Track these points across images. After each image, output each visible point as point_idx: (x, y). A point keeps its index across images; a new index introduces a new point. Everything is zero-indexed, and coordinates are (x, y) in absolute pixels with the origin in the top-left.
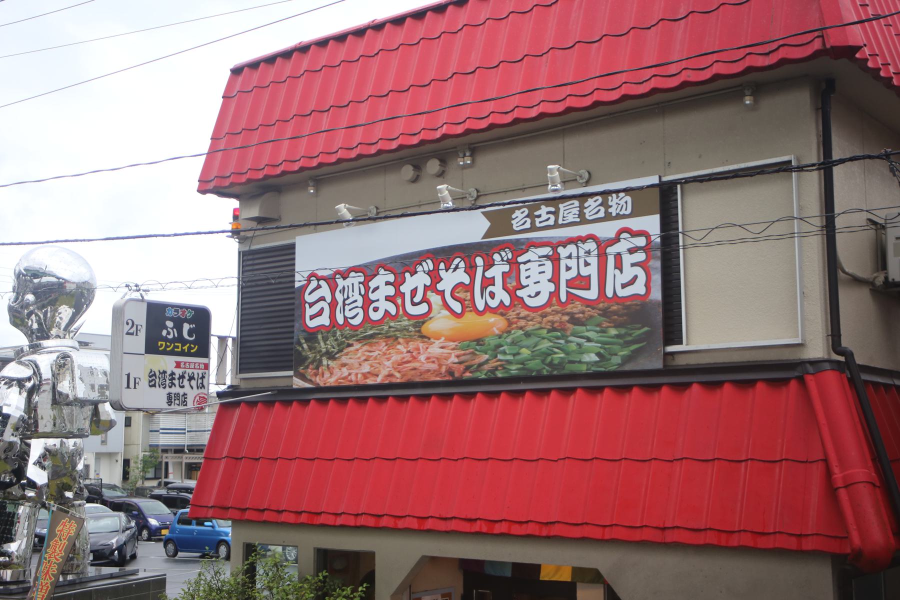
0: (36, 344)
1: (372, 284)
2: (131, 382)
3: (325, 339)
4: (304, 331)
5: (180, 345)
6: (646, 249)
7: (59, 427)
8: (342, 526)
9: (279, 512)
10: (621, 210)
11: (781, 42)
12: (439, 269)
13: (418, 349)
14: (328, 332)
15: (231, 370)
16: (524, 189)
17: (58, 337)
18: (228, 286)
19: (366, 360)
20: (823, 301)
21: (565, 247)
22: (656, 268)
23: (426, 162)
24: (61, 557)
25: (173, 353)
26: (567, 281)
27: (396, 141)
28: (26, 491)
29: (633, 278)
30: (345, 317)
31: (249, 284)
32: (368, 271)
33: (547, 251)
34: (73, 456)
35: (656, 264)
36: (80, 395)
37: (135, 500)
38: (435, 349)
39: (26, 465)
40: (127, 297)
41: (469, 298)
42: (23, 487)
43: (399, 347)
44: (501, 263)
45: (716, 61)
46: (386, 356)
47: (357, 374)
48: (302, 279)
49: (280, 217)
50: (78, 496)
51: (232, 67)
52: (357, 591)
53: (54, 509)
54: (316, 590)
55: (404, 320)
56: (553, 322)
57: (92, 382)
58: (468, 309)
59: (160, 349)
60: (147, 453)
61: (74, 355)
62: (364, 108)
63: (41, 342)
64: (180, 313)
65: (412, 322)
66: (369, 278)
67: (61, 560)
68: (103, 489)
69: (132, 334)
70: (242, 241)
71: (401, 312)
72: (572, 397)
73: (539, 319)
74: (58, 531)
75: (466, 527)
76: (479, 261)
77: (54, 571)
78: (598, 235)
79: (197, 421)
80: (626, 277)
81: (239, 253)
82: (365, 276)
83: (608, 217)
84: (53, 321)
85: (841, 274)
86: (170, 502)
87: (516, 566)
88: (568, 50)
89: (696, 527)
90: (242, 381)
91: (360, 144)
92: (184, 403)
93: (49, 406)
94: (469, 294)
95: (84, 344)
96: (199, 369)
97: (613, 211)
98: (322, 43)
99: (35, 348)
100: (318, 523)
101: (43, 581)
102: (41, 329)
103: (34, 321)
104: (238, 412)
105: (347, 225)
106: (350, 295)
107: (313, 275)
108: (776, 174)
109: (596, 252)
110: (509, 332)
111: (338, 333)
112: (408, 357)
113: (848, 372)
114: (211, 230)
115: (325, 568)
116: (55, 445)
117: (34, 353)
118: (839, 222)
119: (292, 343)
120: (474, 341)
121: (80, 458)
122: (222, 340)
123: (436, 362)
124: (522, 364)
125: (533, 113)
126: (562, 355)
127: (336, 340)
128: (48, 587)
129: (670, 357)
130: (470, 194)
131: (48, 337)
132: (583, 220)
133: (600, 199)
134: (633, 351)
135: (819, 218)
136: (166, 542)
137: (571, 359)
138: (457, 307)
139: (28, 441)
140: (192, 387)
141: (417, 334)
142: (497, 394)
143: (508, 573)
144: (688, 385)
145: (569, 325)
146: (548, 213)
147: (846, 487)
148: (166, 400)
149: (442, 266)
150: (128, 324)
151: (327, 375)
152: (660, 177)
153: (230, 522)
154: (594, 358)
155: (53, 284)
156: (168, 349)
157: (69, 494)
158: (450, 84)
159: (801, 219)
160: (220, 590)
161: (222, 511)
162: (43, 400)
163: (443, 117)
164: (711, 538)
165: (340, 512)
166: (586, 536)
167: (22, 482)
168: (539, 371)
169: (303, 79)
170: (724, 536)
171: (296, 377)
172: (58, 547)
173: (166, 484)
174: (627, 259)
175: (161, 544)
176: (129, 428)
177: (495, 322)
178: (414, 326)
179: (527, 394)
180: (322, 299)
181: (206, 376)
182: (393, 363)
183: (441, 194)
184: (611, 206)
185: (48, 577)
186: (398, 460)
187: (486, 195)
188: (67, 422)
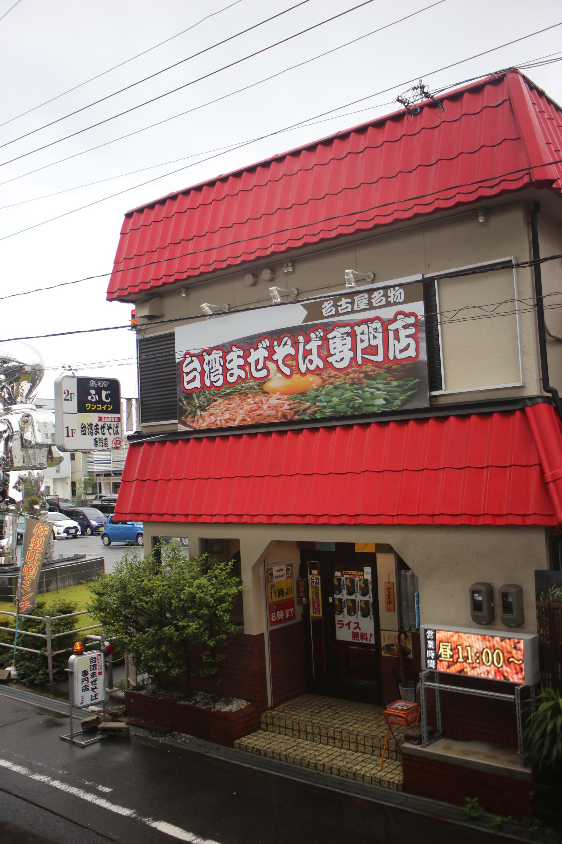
0: (8, 408)
1: (228, 358)
2: (69, 432)
3: (198, 397)
4: (183, 392)
5: (100, 405)
6: (415, 325)
7: (27, 463)
8: (216, 523)
9: (174, 515)
10: (397, 299)
11: (502, 179)
12: (273, 346)
13: (262, 401)
14: (200, 392)
15: (136, 421)
16: (329, 287)
17: (22, 402)
18: (130, 364)
19: (226, 410)
20: (536, 356)
21: (359, 326)
22: (422, 338)
23: (261, 272)
24: (42, 549)
25: (96, 411)
26: (362, 349)
27: (239, 258)
28: (9, 506)
29: (407, 345)
30: (211, 381)
31: (144, 362)
32: (225, 349)
33: (347, 329)
34: (37, 482)
35: (422, 335)
36: (39, 441)
37: (81, 509)
38: (273, 401)
39: (8, 488)
40: (63, 375)
41: (295, 364)
42: (7, 503)
43: (249, 400)
44: (316, 339)
45: (458, 193)
46: (241, 407)
47: (221, 420)
48: (180, 357)
49: (163, 315)
50: (42, 507)
51: (125, 212)
52: (228, 565)
53: (28, 517)
54: (202, 565)
55: (251, 382)
56: (353, 379)
57: (46, 432)
58: (295, 372)
59: (88, 409)
60: (86, 477)
61: (33, 414)
62: (217, 237)
63: (11, 406)
64: (99, 384)
65: (257, 382)
66: (226, 354)
67: (42, 551)
68: (60, 502)
69: (68, 400)
70: (138, 332)
71: (249, 376)
72: (368, 429)
73: (344, 377)
74: (35, 532)
75: (300, 520)
76: (301, 339)
77: (39, 558)
78: (382, 317)
79: (118, 454)
80: (402, 345)
81: (137, 340)
82: (223, 353)
83: (388, 304)
84: (18, 392)
85: (548, 337)
86: (104, 509)
87: (338, 545)
88: (356, 190)
89: (454, 513)
90: (144, 428)
91: (215, 261)
92: (106, 445)
93: (20, 449)
94: (295, 362)
95: (39, 407)
96: (115, 421)
97: (391, 300)
98: (186, 193)
99: (7, 411)
100: (200, 522)
101: (32, 565)
102: (10, 398)
103: (6, 393)
104: (142, 449)
105: (209, 318)
106: (214, 366)
107: (188, 353)
108: (502, 270)
109: (381, 329)
110: (324, 387)
111: (207, 393)
112: (255, 407)
113: (554, 404)
114: (117, 326)
115: (207, 551)
116: (25, 475)
117: (7, 414)
118: (546, 302)
119: (176, 401)
120: (299, 394)
121: (42, 483)
122: (129, 400)
123: (274, 409)
124: (334, 408)
125: (334, 234)
126: (360, 401)
127: (206, 397)
128: (36, 569)
129: (434, 399)
130: (293, 293)
131: (15, 403)
132: (371, 307)
133: (382, 292)
134: (409, 396)
135: (532, 299)
136: (103, 536)
137: (367, 403)
138: (287, 371)
139: (8, 473)
140: (110, 434)
141: (260, 391)
142: (317, 429)
143: (333, 549)
144: (447, 418)
145: (364, 380)
146: (347, 303)
147: (554, 481)
148: (93, 443)
149: (275, 343)
150: (65, 393)
151: (201, 421)
152: (423, 275)
153: (142, 523)
154: (382, 402)
155: (16, 367)
156: (93, 409)
157: (37, 507)
158: (275, 217)
159: (519, 301)
160: (138, 568)
161: (136, 516)
162: (15, 445)
163: (272, 239)
164: (464, 520)
165: (214, 514)
166: (381, 522)
167: (6, 500)
168: (345, 412)
169: (174, 217)
170: (473, 518)
171: (180, 424)
172: (38, 542)
173: (101, 497)
174: (403, 333)
175: (100, 537)
176: (73, 461)
177: (313, 380)
178: (258, 385)
179: (338, 429)
180: (195, 369)
181: (119, 426)
182: (245, 412)
183: (272, 293)
184: (390, 297)
185: (35, 562)
186: (251, 477)
187: (303, 292)
188: (32, 459)
